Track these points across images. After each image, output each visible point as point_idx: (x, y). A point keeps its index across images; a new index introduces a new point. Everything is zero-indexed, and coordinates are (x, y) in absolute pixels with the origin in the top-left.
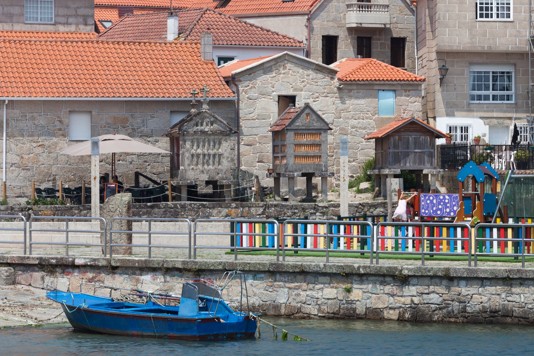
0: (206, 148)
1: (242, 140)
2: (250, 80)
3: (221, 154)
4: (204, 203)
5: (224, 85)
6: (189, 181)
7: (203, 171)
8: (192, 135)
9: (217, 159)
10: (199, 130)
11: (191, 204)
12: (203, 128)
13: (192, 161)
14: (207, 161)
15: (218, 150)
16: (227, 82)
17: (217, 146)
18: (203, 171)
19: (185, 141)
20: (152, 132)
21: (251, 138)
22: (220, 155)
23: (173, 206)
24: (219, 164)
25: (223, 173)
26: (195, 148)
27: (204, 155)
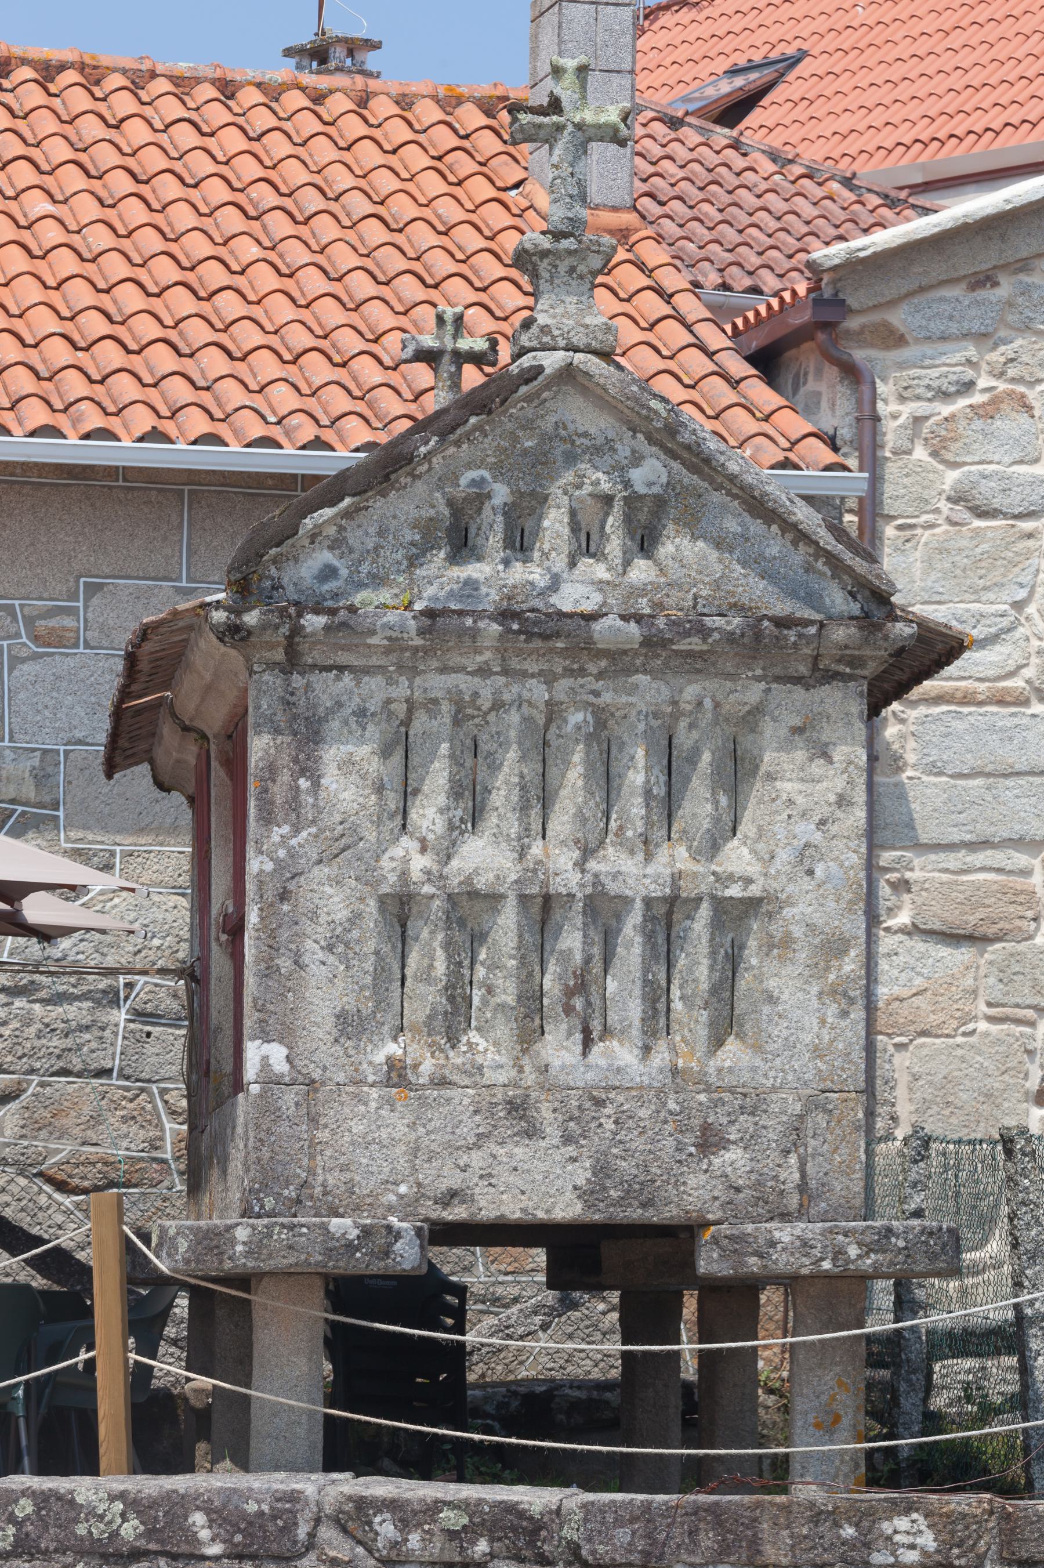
0: (561, 823)
1: (902, 886)
2: (982, 337)
3: (751, 905)
4: (535, 1498)
5: (734, 383)
6: (343, 1226)
7: (518, 1108)
8: (403, 656)
9: (696, 965)
10: (491, 598)
11: (362, 1506)
12: (528, 574)
13: (391, 976)
14: (581, 984)
15: (714, 847)
16: (768, 362)
17: (699, 806)
18: (518, 1108)
19: (308, 733)
20: (42, 778)
21: (981, 873)
22: (736, 915)
23: (130, 1530)
24: (725, 1024)
25: (773, 1127)
26: (429, 815)
27: (543, 910)
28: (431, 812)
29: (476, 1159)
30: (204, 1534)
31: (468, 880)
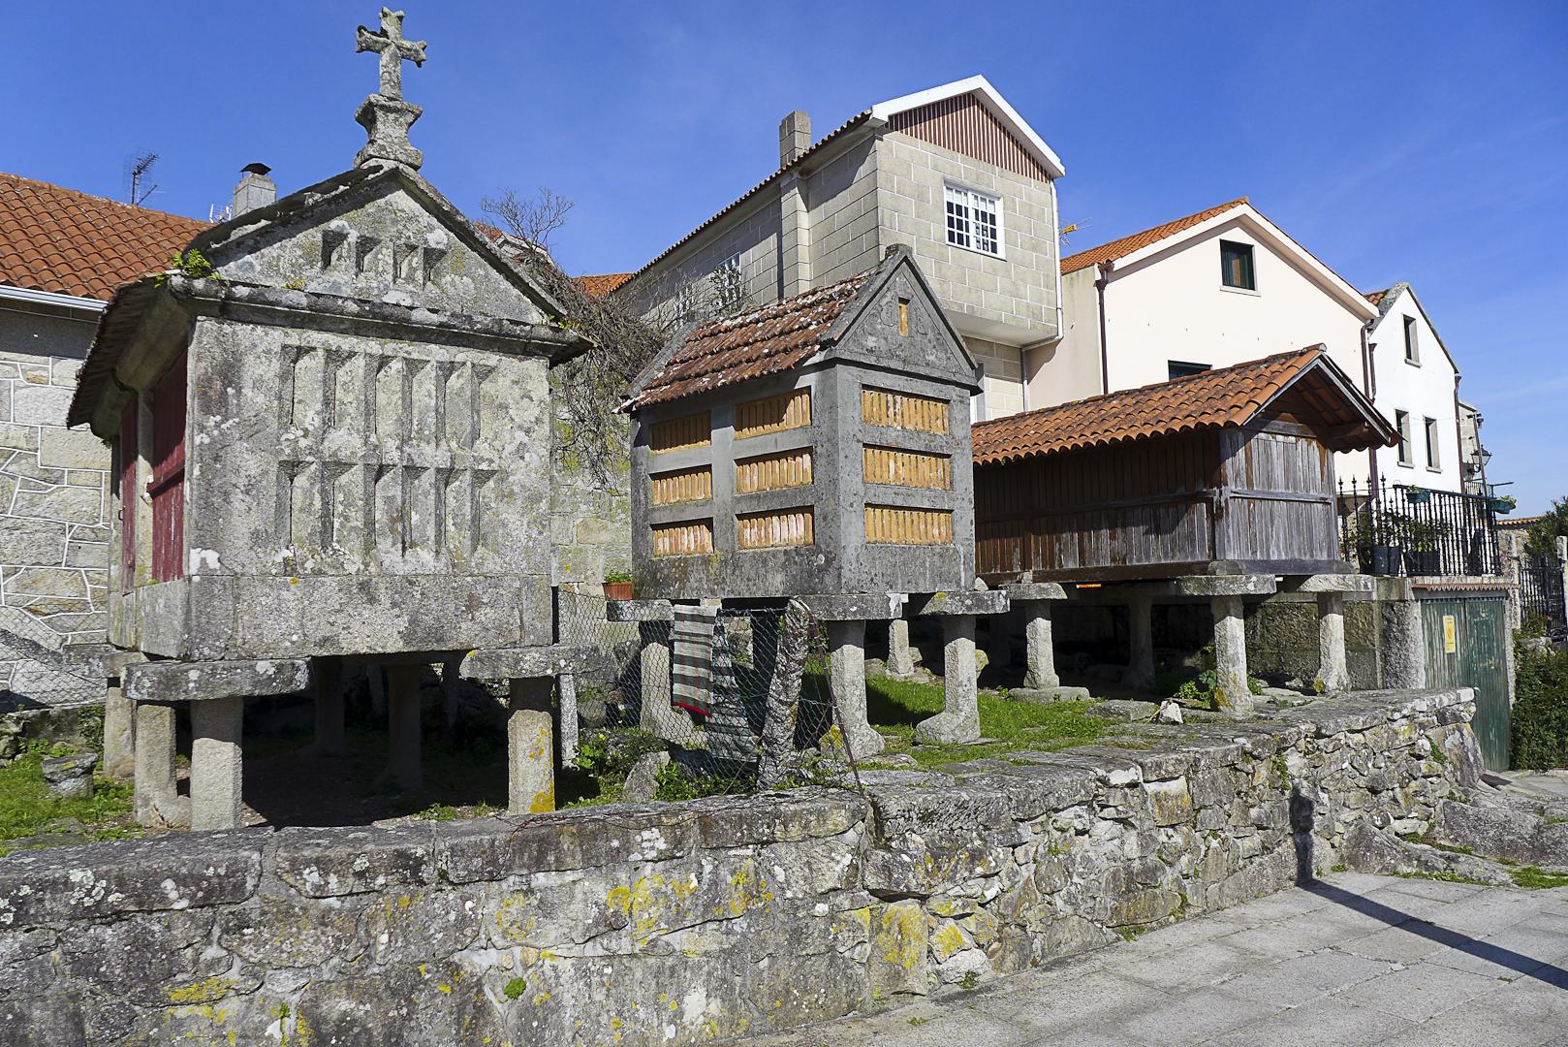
6: (264, 667)
7: (364, 586)
20: (28, 438)
28: (311, 414)
29: (341, 619)
30: (173, 895)
31: (335, 454)
